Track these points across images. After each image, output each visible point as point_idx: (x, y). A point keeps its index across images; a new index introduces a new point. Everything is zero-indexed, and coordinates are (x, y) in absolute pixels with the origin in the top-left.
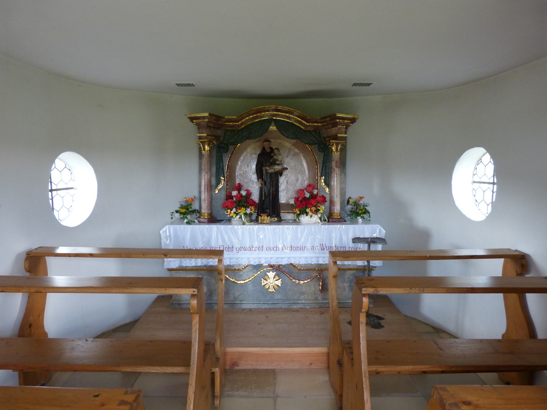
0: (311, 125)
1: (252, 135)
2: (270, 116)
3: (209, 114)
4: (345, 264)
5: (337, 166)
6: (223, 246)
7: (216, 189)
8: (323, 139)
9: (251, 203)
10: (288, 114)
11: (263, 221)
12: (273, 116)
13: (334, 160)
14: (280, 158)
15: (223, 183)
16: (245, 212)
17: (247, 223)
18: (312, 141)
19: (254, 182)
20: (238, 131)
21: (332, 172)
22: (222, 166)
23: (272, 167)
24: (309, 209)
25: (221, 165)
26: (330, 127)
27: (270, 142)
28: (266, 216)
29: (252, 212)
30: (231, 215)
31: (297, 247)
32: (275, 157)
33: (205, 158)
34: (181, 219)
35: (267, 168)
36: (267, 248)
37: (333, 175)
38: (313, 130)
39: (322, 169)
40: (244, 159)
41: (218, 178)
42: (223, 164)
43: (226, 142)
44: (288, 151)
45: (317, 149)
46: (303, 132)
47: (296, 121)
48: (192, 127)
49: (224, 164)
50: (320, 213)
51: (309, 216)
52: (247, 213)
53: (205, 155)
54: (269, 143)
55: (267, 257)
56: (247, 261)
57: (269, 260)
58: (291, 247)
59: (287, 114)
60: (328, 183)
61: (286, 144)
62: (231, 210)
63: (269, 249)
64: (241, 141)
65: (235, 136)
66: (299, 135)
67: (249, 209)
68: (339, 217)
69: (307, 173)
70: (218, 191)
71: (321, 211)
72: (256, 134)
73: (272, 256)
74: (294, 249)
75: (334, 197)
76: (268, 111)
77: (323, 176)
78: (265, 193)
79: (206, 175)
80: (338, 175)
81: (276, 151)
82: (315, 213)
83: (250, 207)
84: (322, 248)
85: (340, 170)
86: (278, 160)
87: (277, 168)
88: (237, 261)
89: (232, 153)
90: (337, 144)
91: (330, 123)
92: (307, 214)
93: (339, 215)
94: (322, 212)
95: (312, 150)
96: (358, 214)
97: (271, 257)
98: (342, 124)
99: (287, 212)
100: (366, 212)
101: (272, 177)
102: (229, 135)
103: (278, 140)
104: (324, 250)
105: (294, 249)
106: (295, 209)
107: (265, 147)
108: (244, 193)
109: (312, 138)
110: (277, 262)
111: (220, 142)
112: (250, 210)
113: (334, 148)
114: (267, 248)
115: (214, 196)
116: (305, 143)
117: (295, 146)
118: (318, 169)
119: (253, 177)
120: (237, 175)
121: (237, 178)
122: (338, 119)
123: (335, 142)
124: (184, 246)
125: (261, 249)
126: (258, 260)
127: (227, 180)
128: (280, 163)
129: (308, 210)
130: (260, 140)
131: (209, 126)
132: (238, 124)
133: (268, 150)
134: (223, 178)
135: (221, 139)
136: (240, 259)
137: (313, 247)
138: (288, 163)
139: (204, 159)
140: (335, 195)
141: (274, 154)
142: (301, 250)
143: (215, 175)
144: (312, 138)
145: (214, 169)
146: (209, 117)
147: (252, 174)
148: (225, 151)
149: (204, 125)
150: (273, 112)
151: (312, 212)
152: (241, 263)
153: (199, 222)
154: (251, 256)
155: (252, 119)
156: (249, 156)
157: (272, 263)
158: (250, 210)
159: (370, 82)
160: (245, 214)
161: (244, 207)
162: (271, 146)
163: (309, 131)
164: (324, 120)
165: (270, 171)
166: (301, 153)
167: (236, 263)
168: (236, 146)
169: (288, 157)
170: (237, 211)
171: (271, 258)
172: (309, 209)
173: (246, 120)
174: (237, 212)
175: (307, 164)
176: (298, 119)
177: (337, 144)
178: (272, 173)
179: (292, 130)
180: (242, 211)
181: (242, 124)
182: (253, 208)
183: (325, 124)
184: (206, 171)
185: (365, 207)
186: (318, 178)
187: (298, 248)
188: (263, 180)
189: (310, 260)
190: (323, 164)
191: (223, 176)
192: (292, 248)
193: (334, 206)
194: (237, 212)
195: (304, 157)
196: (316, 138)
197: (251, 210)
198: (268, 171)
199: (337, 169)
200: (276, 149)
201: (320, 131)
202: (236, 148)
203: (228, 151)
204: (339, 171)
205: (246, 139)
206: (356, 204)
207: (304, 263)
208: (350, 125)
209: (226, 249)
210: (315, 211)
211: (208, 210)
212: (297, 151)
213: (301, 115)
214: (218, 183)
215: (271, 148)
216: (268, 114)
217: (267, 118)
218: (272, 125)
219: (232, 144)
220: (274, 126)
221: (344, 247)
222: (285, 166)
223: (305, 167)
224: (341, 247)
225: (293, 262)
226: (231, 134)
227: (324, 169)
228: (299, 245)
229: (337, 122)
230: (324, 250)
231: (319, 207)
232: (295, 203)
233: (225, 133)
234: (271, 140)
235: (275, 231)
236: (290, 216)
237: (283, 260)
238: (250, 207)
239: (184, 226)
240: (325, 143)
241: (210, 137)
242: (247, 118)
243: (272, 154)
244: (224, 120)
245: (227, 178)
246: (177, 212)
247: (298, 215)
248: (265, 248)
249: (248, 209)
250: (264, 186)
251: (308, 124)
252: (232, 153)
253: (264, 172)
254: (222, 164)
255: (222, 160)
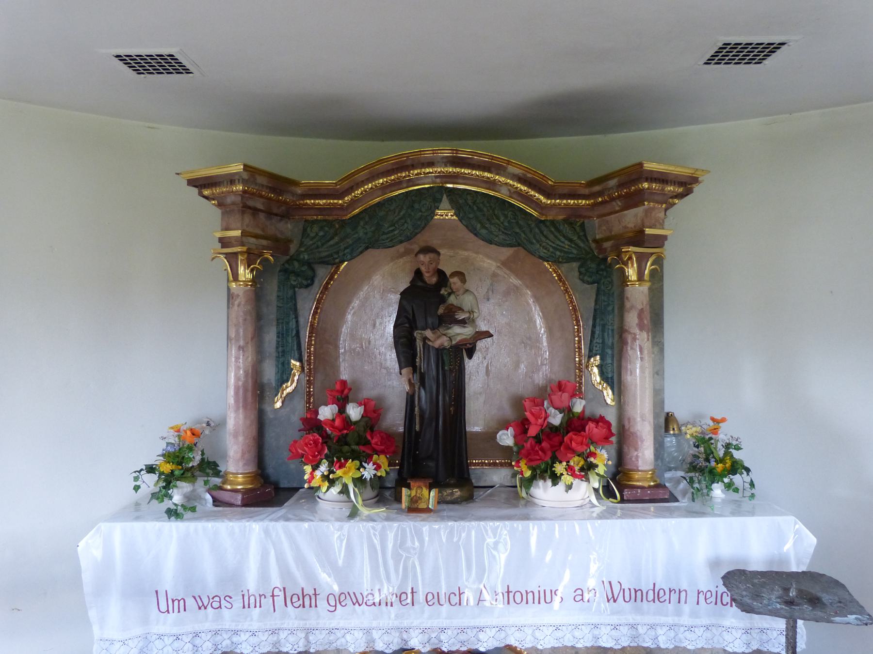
0: (560, 204)
1: (385, 237)
2: (438, 180)
3: (246, 167)
4: (685, 648)
5: (641, 327)
6: (284, 589)
7: (276, 395)
8: (593, 245)
9: (376, 444)
10: (489, 171)
11: (417, 502)
12: (444, 180)
13: (632, 307)
14: (467, 301)
15: (296, 378)
16: (358, 475)
17: (364, 511)
18: (561, 251)
19: (391, 373)
20: (343, 224)
21: (626, 343)
22: (294, 326)
23: (442, 330)
24: (564, 463)
25: (293, 324)
26: (617, 208)
27: (439, 254)
28: (426, 486)
29: (379, 474)
30: (314, 484)
31: (527, 593)
32: (452, 300)
33: (236, 303)
34: (151, 499)
35: (428, 333)
36: (430, 597)
37: (630, 352)
38: (564, 220)
39: (593, 333)
40: (363, 305)
41: (283, 364)
42: (297, 322)
43: (306, 257)
44: (488, 282)
45: (577, 274)
46: (533, 225)
47: (514, 192)
48: (210, 212)
49: (301, 320)
50: (598, 474)
51: (561, 486)
52: (365, 479)
53: (238, 296)
54: (432, 255)
55: (428, 625)
56: (364, 639)
57: (433, 635)
58: (508, 592)
59: (486, 174)
60: (610, 376)
61: (484, 262)
62: (315, 468)
63: (433, 599)
64: (353, 251)
65: (332, 238)
66: (523, 235)
67: (371, 464)
68: (652, 484)
69: (545, 344)
70: (283, 402)
71: (601, 470)
72: (396, 232)
73: (444, 623)
74: (518, 599)
75: (635, 419)
76: (431, 164)
77: (596, 355)
78: (420, 408)
79: (241, 357)
80: (646, 352)
81: (455, 281)
82: (583, 476)
83: (375, 457)
84: (610, 596)
85: (650, 338)
86: (461, 309)
87: (459, 333)
88: (331, 638)
89: (326, 288)
90: (642, 259)
91: (619, 197)
92: (555, 479)
93: (652, 478)
94: (602, 473)
95: (560, 279)
96: (714, 476)
97: (441, 626)
98: (656, 198)
99: (489, 464)
100: (736, 467)
101: (443, 360)
102: (317, 235)
103: (461, 252)
104: (615, 601)
105: (518, 597)
106: (518, 462)
107: (423, 269)
108: (354, 412)
109: (558, 242)
110: (462, 643)
111: (288, 257)
112: (375, 469)
113: (632, 272)
114: (430, 597)
115: (270, 415)
116: (541, 257)
117: (510, 269)
118: (581, 334)
119: (388, 357)
120: (342, 351)
121: (344, 360)
122: (647, 180)
123: (635, 253)
124: (157, 592)
125: (409, 600)
126: (398, 634)
127: (310, 369)
128: (469, 318)
129: (559, 468)
130: (407, 252)
131: (250, 208)
132: (340, 202)
133: (431, 279)
134: (298, 364)
135: (293, 249)
136: (339, 634)
137: (579, 592)
138: (488, 317)
139: (236, 307)
140: (639, 416)
141: (450, 291)
142: (539, 603)
143: (275, 354)
144: (563, 242)
145: (271, 337)
146: (245, 176)
147: (386, 348)
148: (305, 282)
149: (233, 204)
150: (446, 166)
151: (574, 475)
152: (342, 645)
153: (217, 502)
154: (374, 624)
155: (384, 188)
156: (377, 296)
157: (446, 645)
158: (375, 469)
159: (776, 39)
160: (359, 481)
161: (355, 456)
162: (440, 267)
163: (553, 222)
164: (597, 188)
165: (437, 344)
166: (527, 287)
167: (327, 647)
168: (338, 268)
169: (488, 300)
170: (333, 472)
171: (443, 630)
172: (564, 463)
173: (366, 191)
174: (331, 476)
175: (545, 317)
176: (519, 185)
177: (642, 259)
178: (444, 349)
179: (502, 219)
180: (348, 473)
181: (354, 203)
182: (383, 460)
183: (600, 199)
184: (242, 343)
185: (731, 450)
186: (580, 361)
187: (530, 596)
188: (415, 369)
189: (569, 636)
190: (595, 319)
191: (297, 356)
192: (511, 595)
193: (636, 450)
194: (331, 476)
195: (537, 299)
196: (571, 240)
197: (378, 467)
198: (430, 343)
199: (644, 335)
200: (454, 274)
201: (583, 222)
202: (335, 272)
203: (312, 284)
204: (648, 340)
205: (367, 248)
206: (704, 441)
207: (549, 646)
208: (675, 204)
209: (295, 599)
210: (582, 469)
211: (245, 465)
212: (514, 281)
213: (529, 175)
214: (282, 378)
215: (441, 273)
216: (430, 173)
217: (426, 186)
218: (441, 206)
219: (324, 262)
220: (450, 207)
221: (680, 592)
222: (483, 327)
223: (539, 327)
224: (670, 591)
225: (513, 642)
226: (321, 234)
227: (597, 332)
228: (533, 586)
229: (643, 190)
230: (615, 601)
231: (593, 455)
232: (516, 444)
233: (305, 230)
234: (442, 251)
235: (455, 540)
236: (499, 476)
237: (481, 636)
238: (375, 457)
239: (158, 525)
240: (601, 256)
241: (252, 240)
242: (367, 184)
243: (443, 292)
244: (299, 191)
245: (309, 364)
246: (151, 469)
247: (528, 483)
248: (420, 597)
249: (365, 465)
250: (419, 389)
251: (549, 202)
252: (326, 288)
253: (419, 344)
254: (294, 320)
255: (295, 310)
